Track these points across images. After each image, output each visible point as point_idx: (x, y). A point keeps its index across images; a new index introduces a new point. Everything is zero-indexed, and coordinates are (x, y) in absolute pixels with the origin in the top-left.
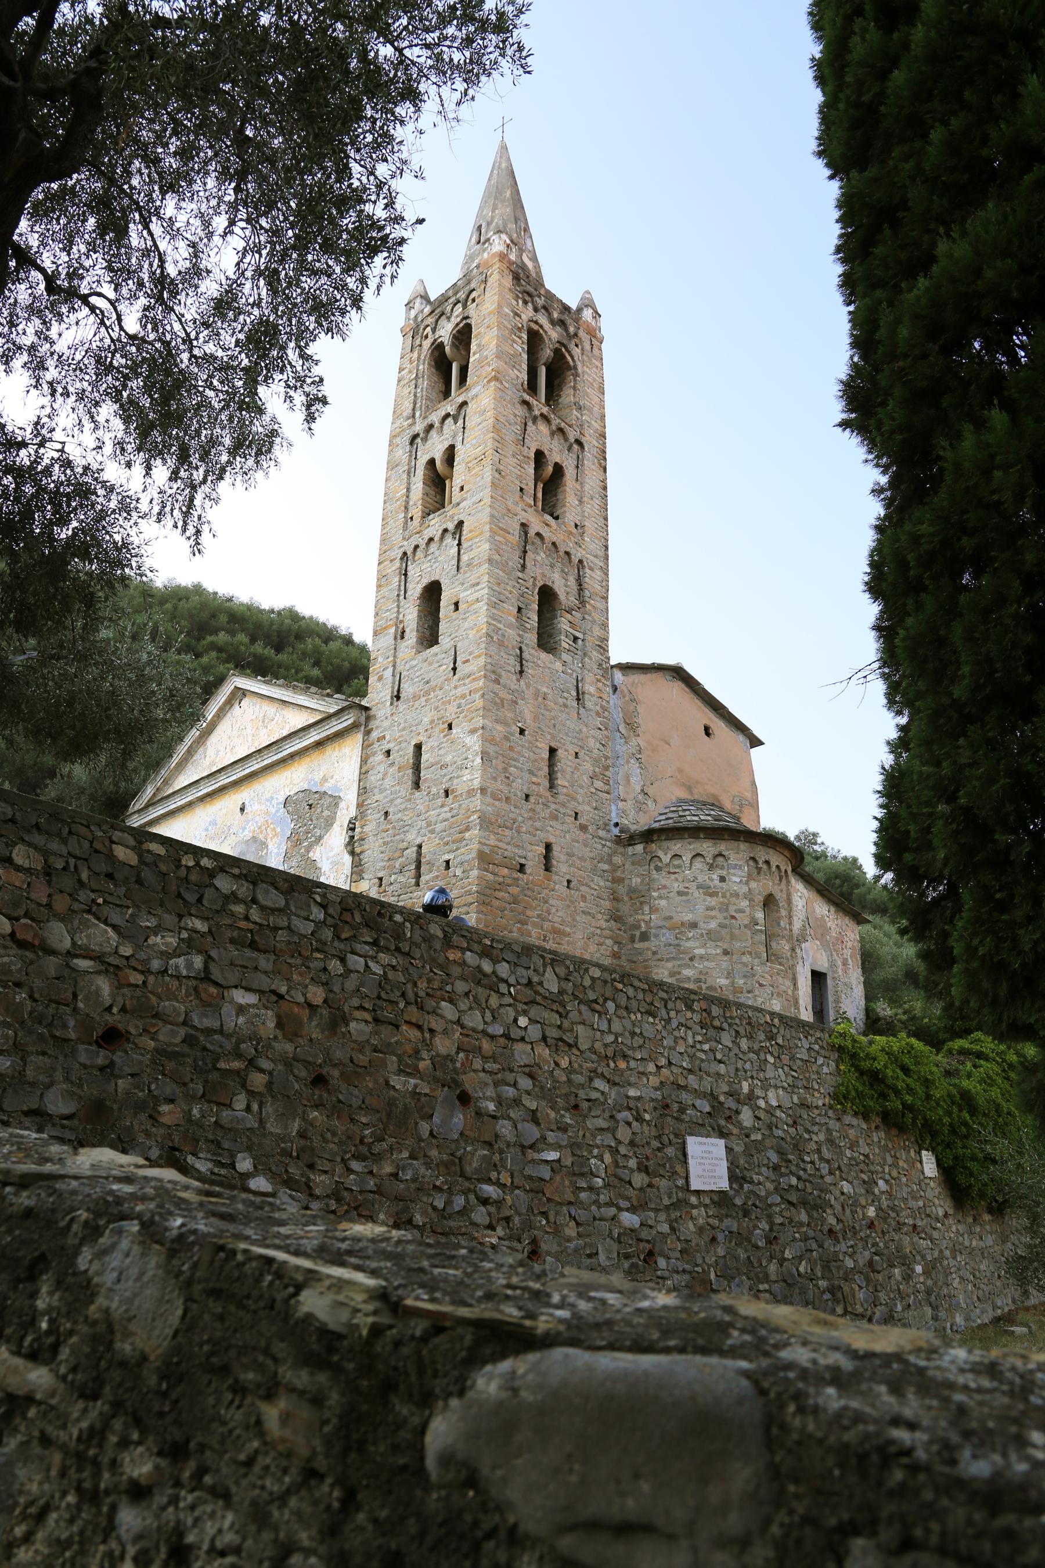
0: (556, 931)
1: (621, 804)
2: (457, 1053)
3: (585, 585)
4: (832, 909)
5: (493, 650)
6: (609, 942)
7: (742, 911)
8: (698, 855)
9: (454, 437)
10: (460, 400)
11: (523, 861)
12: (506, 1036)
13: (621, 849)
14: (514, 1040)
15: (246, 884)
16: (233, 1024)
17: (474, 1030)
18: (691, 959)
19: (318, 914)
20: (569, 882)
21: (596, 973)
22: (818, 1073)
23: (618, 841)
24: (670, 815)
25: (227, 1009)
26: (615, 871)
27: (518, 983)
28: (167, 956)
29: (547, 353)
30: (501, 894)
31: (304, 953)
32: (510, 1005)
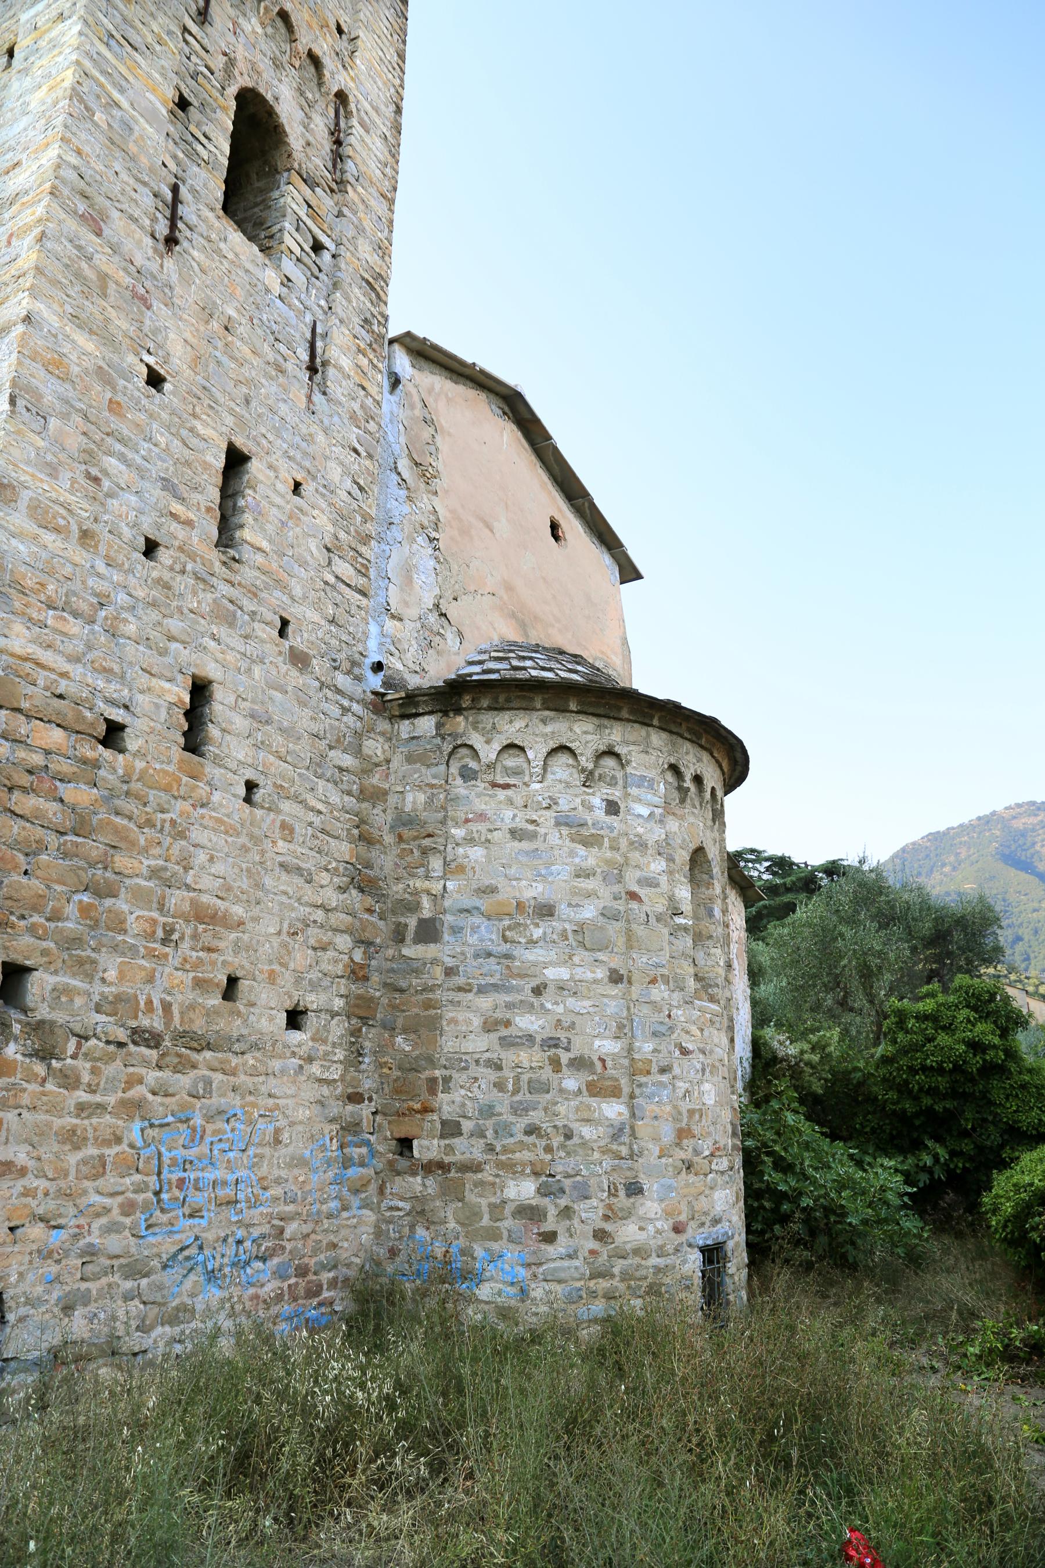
0: (202, 916)
1: (390, 625)
3: (347, 151)
5: (92, 144)
6: (344, 942)
7: (650, 883)
8: (563, 748)
11: (118, 715)
13: (383, 725)
18: (537, 991)
20: (251, 786)
23: (379, 703)
24: (492, 665)
26: (366, 772)
30: (28, 803)
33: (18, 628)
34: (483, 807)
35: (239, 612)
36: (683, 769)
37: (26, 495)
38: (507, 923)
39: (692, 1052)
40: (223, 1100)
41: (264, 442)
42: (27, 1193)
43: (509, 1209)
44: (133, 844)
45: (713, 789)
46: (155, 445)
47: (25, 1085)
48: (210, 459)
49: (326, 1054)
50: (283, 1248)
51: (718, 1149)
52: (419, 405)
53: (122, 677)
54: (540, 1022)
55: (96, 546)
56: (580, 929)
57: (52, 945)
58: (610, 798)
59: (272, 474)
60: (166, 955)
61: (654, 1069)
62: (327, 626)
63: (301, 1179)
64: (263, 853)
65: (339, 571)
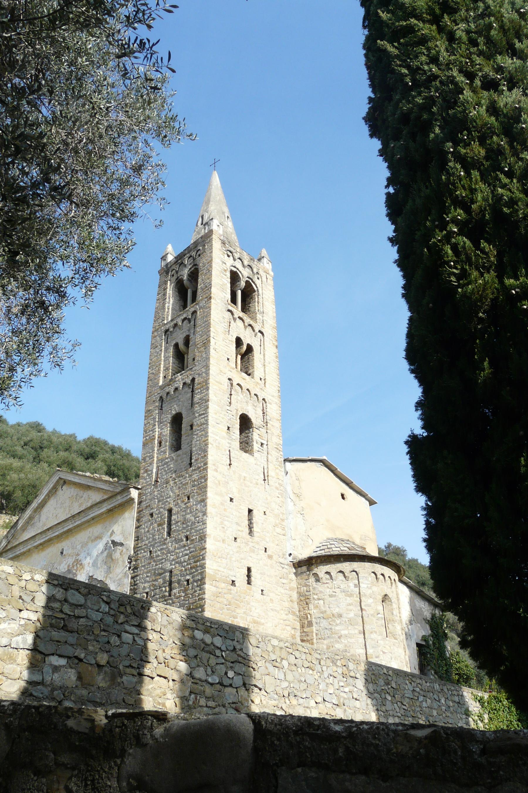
1: (293, 543)
2: (190, 695)
4: (427, 603)
6: (289, 628)
9: (189, 330)
10: (193, 309)
12: (221, 684)
14: (225, 686)
15: (61, 590)
16: (50, 678)
17: (200, 680)
18: (339, 637)
19: (105, 608)
20: (262, 591)
21: (275, 642)
22: (420, 707)
25: (47, 669)
27: (227, 650)
28: (13, 635)
29: (243, 284)
30: (220, 600)
31: (95, 632)
32: (222, 664)
56: (350, 620)
61: (374, 656)
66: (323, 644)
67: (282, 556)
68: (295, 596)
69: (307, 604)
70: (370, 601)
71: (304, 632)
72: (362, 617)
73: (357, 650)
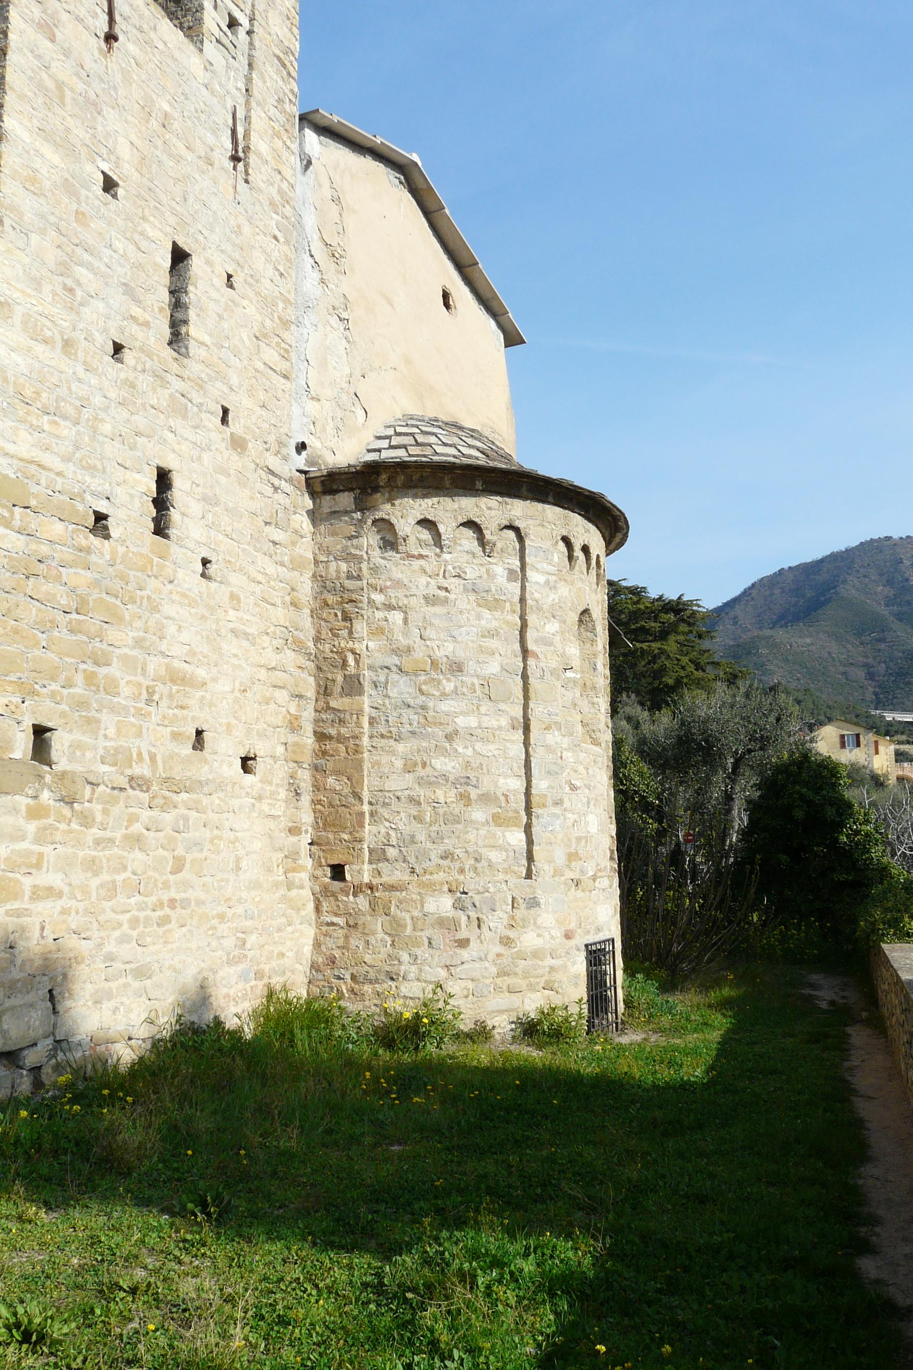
0: (175, 678)
1: (312, 407)
6: (282, 696)
20: (205, 562)
30: (45, 588)
33: (23, 434)
34: (400, 576)
35: (189, 404)
36: (573, 540)
37: (19, 311)
38: (423, 678)
39: (579, 788)
40: (197, 834)
41: (201, 237)
42: (64, 912)
43: (430, 920)
44: (121, 619)
45: (598, 556)
46: (114, 251)
47: (58, 825)
48: (159, 260)
49: (272, 793)
50: (245, 956)
51: (600, 870)
52: (326, 183)
53: (104, 472)
54: (453, 764)
55: (76, 354)
56: (486, 683)
57: (67, 708)
58: (511, 567)
59: (209, 269)
60: (150, 714)
61: (549, 801)
62: (260, 411)
63: (257, 899)
64: (217, 621)
65: (267, 358)
66: (393, 753)
67: (274, 447)
68: (306, 588)
69: (346, 618)
70: (552, 627)
71: (328, 708)
72: (525, 676)
73: (501, 781)
